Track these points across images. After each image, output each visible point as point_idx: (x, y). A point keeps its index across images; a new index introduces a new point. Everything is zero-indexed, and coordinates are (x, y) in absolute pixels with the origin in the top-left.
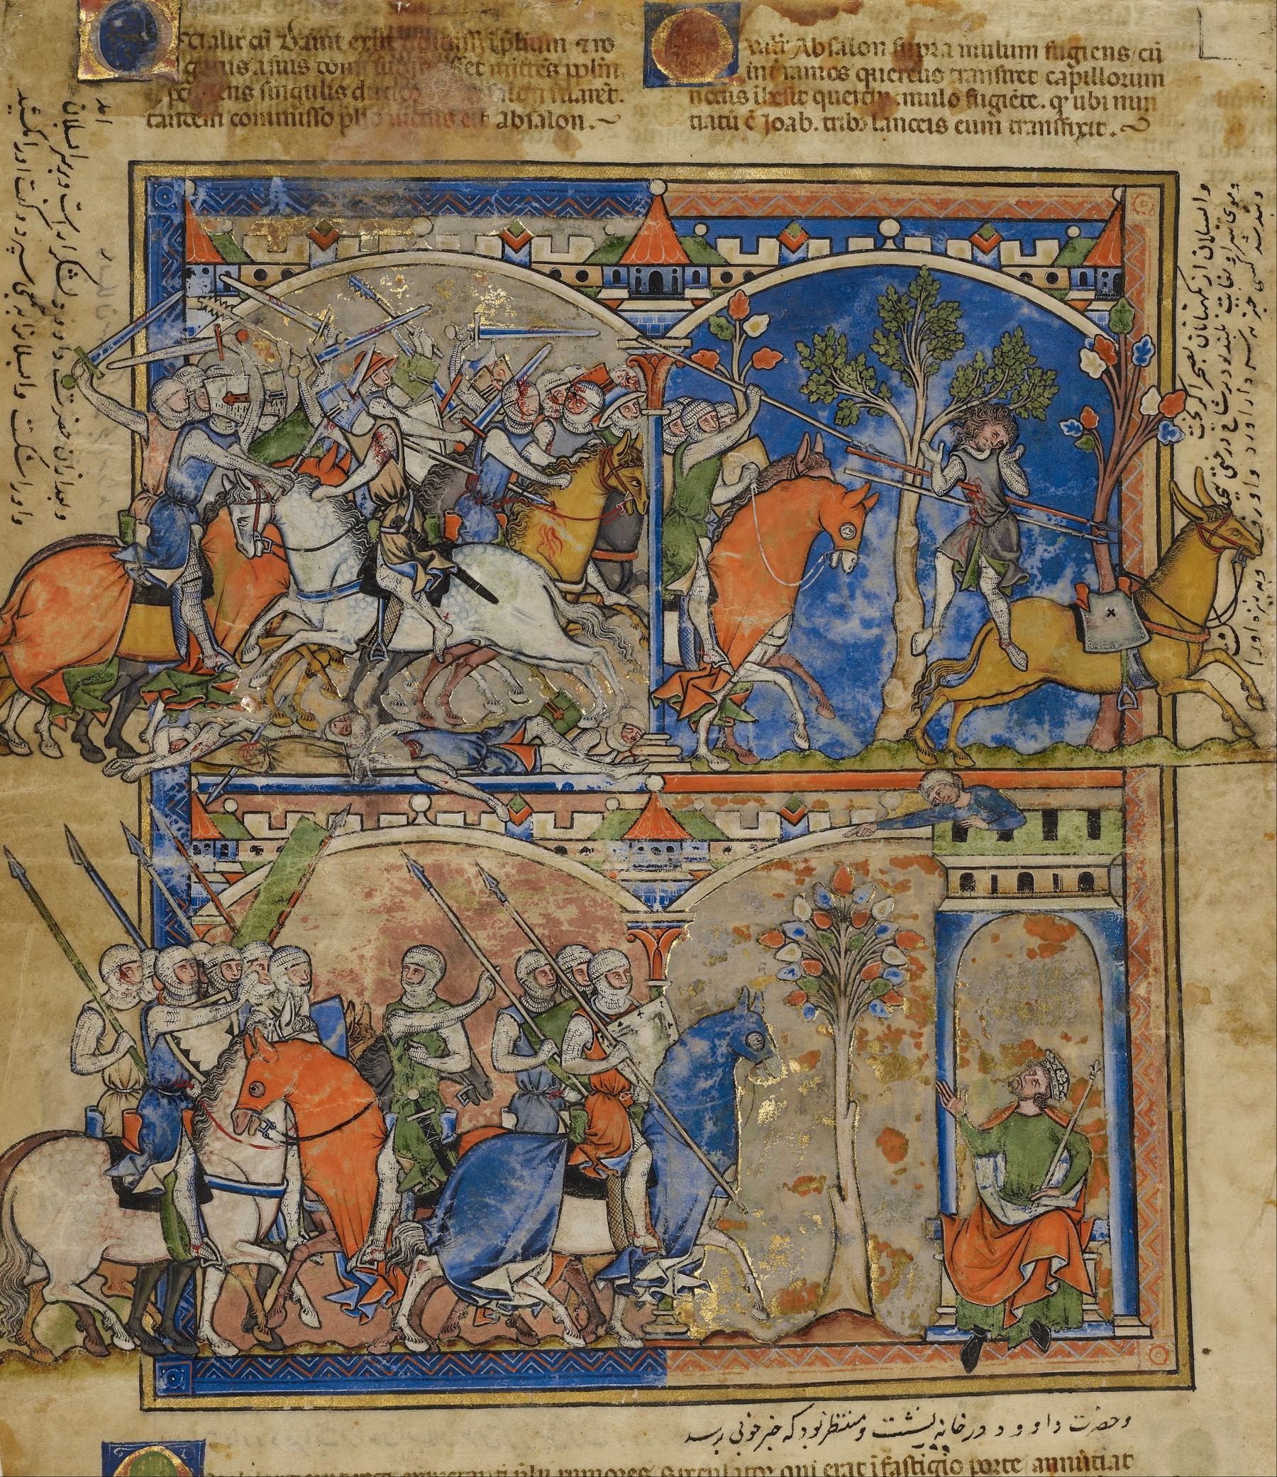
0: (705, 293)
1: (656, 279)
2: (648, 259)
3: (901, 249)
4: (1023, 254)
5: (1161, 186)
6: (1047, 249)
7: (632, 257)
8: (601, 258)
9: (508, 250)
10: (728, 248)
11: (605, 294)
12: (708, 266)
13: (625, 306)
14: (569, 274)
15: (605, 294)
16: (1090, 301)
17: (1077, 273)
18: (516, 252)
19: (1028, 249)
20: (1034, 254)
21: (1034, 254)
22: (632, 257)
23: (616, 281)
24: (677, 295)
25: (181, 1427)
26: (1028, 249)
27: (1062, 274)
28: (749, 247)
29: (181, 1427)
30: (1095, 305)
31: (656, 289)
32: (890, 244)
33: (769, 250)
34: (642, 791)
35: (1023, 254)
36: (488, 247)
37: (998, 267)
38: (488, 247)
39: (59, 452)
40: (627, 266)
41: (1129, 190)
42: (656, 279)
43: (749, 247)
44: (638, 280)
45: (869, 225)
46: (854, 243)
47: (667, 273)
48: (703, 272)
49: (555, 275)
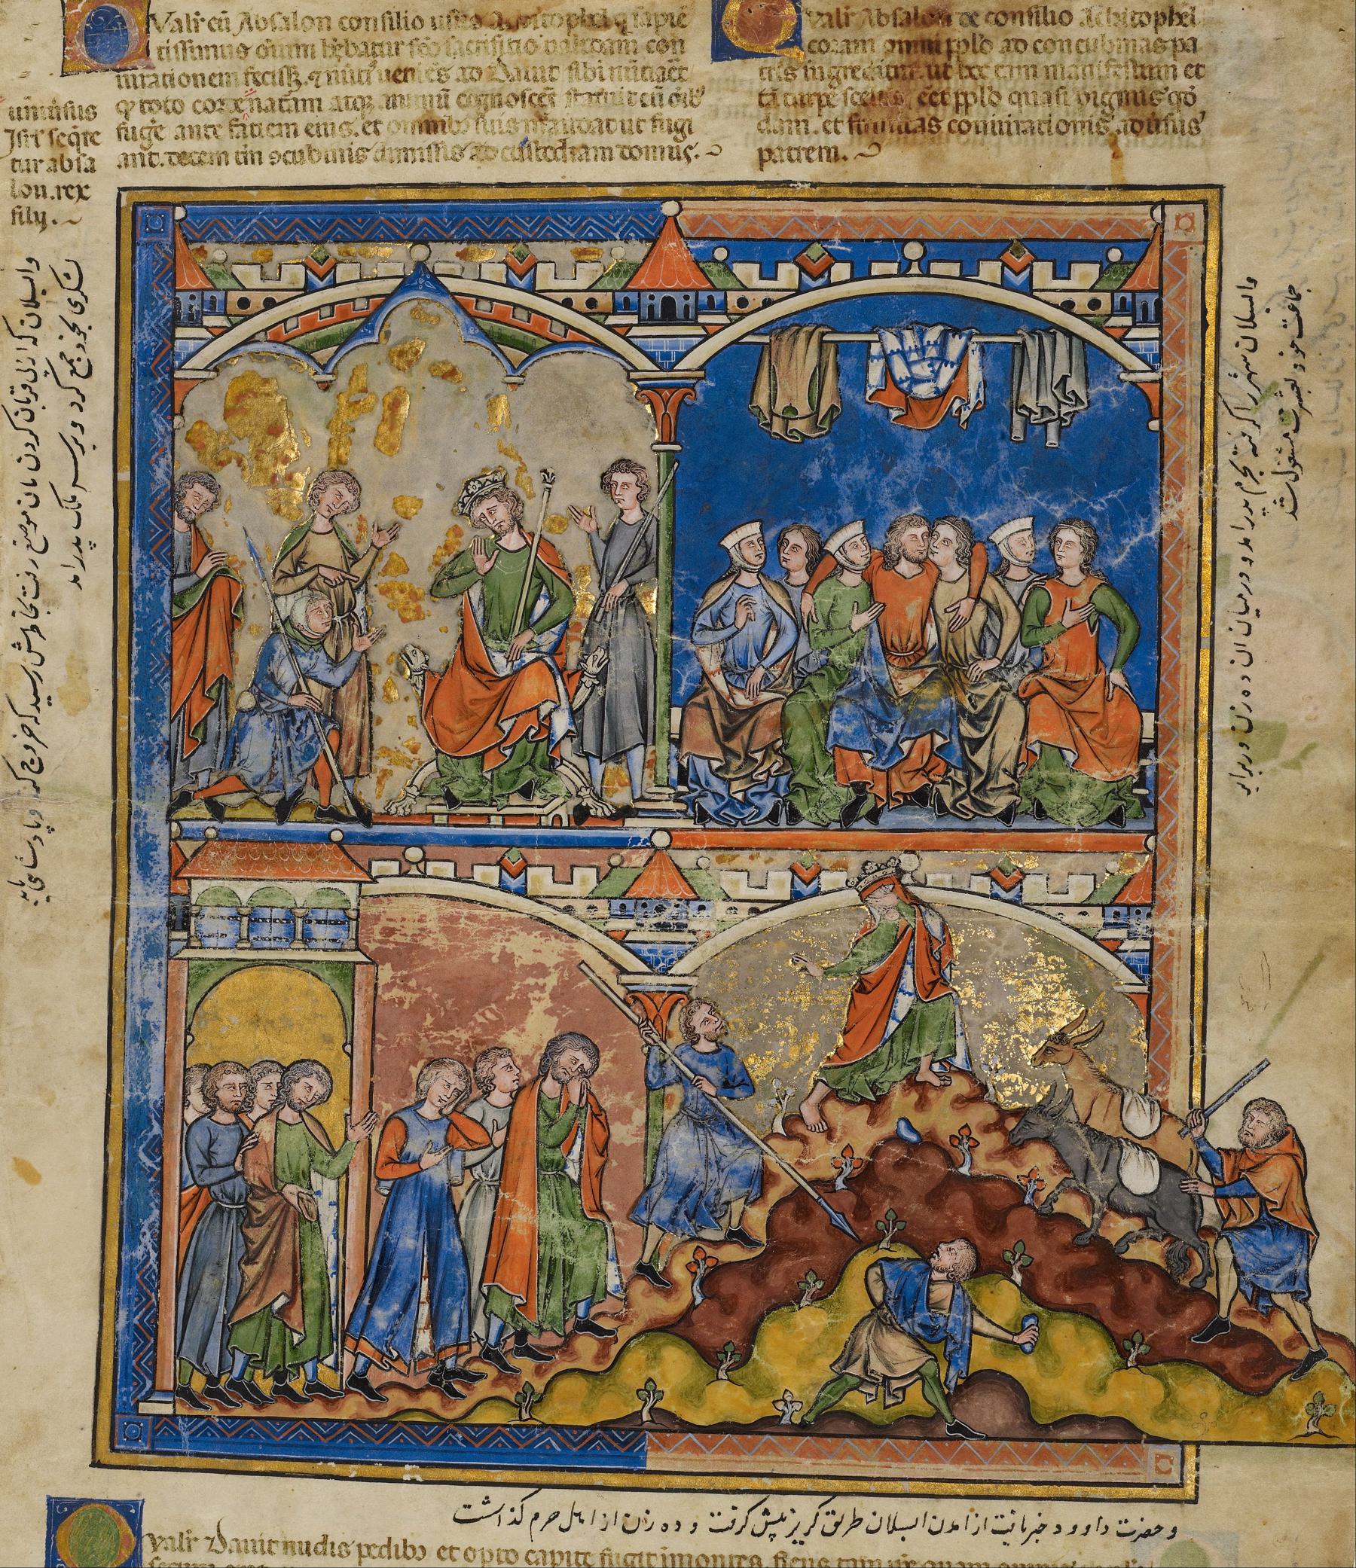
0: (723, 319)
1: (668, 303)
2: (661, 283)
3: (927, 274)
4: (761, 278)
5: (1204, 202)
6: (1085, 274)
7: (642, 282)
8: (606, 283)
9: (513, 276)
10: (747, 272)
11: (612, 320)
12: (725, 290)
13: (634, 332)
14: (580, 300)
15: (612, 320)
16: (1129, 329)
17: (1118, 297)
18: (1017, 274)
19: (1061, 272)
20: (775, 278)
21: (775, 278)
22: (642, 282)
23: (626, 307)
24: (689, 320)
25: (120, 1485)
26: (1061, 272)
27: (1105, 298)
28: (769, 272)
29: (120, 1485)
30: (1134, 333)
31: (668, 314)
32: (915, 270)
33: (788, 274)
34: (581, 671)
35: (761, 278)
36: (484, 875)
37: (1028, 290)
38: (484, 875)
39: (33, 501)
40: (639, 291)
41: (1168, 209)
42: (668, 303)
43: (769, 272)
44: (651, 308)
45: (891, 247)
46: (877, 269)
47: (679, 299)
48: (718, 297)
49: (567, 303)
